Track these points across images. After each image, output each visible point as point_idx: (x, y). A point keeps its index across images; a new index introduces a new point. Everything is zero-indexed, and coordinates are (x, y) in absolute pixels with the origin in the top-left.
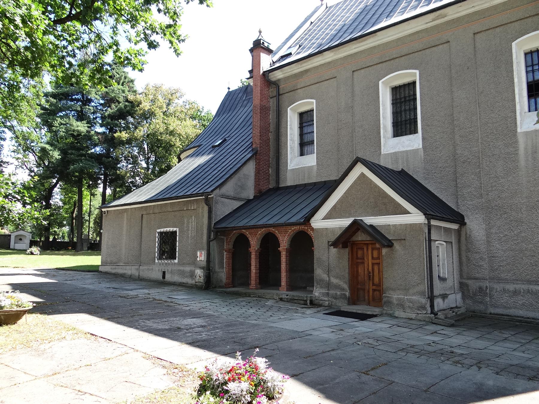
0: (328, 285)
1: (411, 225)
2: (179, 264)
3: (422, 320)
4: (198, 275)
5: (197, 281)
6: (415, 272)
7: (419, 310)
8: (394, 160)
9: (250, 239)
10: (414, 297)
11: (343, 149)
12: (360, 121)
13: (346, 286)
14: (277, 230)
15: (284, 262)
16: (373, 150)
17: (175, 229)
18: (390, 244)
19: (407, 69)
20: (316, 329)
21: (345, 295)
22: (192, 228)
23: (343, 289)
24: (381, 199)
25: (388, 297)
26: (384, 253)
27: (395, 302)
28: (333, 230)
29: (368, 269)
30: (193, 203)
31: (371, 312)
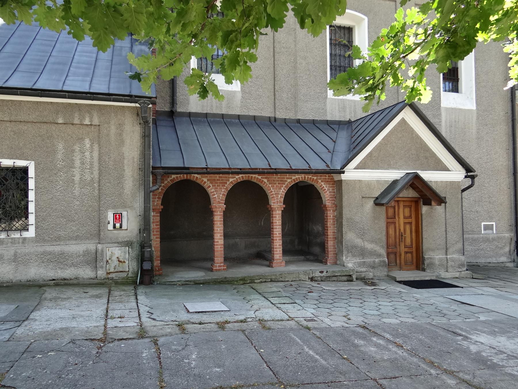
0: (362, 253)
1: (451, 182)
2: (39, 238)
3: (465, 277)
4: (114, 258)
5: (112, 270)
6: (454, 230)
7: (459, 268)
8: (341, 108)
9: (211, 190)
10: (454, 256)
11: (282, 79)
12: (303, 51)
13: (383, 252)
14: (266, 178)
15: (279, 225)
16: (319, 91)
17: (21, 163)
18: (441, 201)
19: (356, 11)
20: (481, 310)
21: (384, 262)
22: (83, 163)
23: (380, 255)
24: (423, 151)
25: (431, 258)
26: (424, 211)
27: (437, 262)
28: (368, 184)
29: (400, 230)
30: (89, 112)
31: (429, 278)
